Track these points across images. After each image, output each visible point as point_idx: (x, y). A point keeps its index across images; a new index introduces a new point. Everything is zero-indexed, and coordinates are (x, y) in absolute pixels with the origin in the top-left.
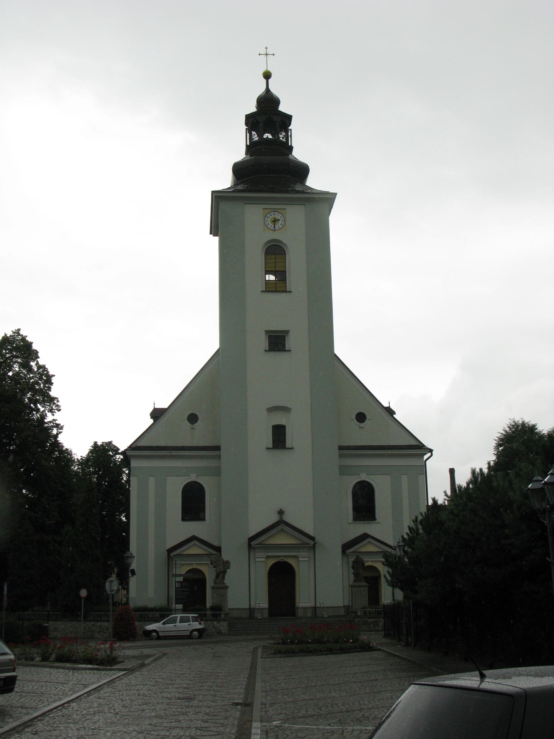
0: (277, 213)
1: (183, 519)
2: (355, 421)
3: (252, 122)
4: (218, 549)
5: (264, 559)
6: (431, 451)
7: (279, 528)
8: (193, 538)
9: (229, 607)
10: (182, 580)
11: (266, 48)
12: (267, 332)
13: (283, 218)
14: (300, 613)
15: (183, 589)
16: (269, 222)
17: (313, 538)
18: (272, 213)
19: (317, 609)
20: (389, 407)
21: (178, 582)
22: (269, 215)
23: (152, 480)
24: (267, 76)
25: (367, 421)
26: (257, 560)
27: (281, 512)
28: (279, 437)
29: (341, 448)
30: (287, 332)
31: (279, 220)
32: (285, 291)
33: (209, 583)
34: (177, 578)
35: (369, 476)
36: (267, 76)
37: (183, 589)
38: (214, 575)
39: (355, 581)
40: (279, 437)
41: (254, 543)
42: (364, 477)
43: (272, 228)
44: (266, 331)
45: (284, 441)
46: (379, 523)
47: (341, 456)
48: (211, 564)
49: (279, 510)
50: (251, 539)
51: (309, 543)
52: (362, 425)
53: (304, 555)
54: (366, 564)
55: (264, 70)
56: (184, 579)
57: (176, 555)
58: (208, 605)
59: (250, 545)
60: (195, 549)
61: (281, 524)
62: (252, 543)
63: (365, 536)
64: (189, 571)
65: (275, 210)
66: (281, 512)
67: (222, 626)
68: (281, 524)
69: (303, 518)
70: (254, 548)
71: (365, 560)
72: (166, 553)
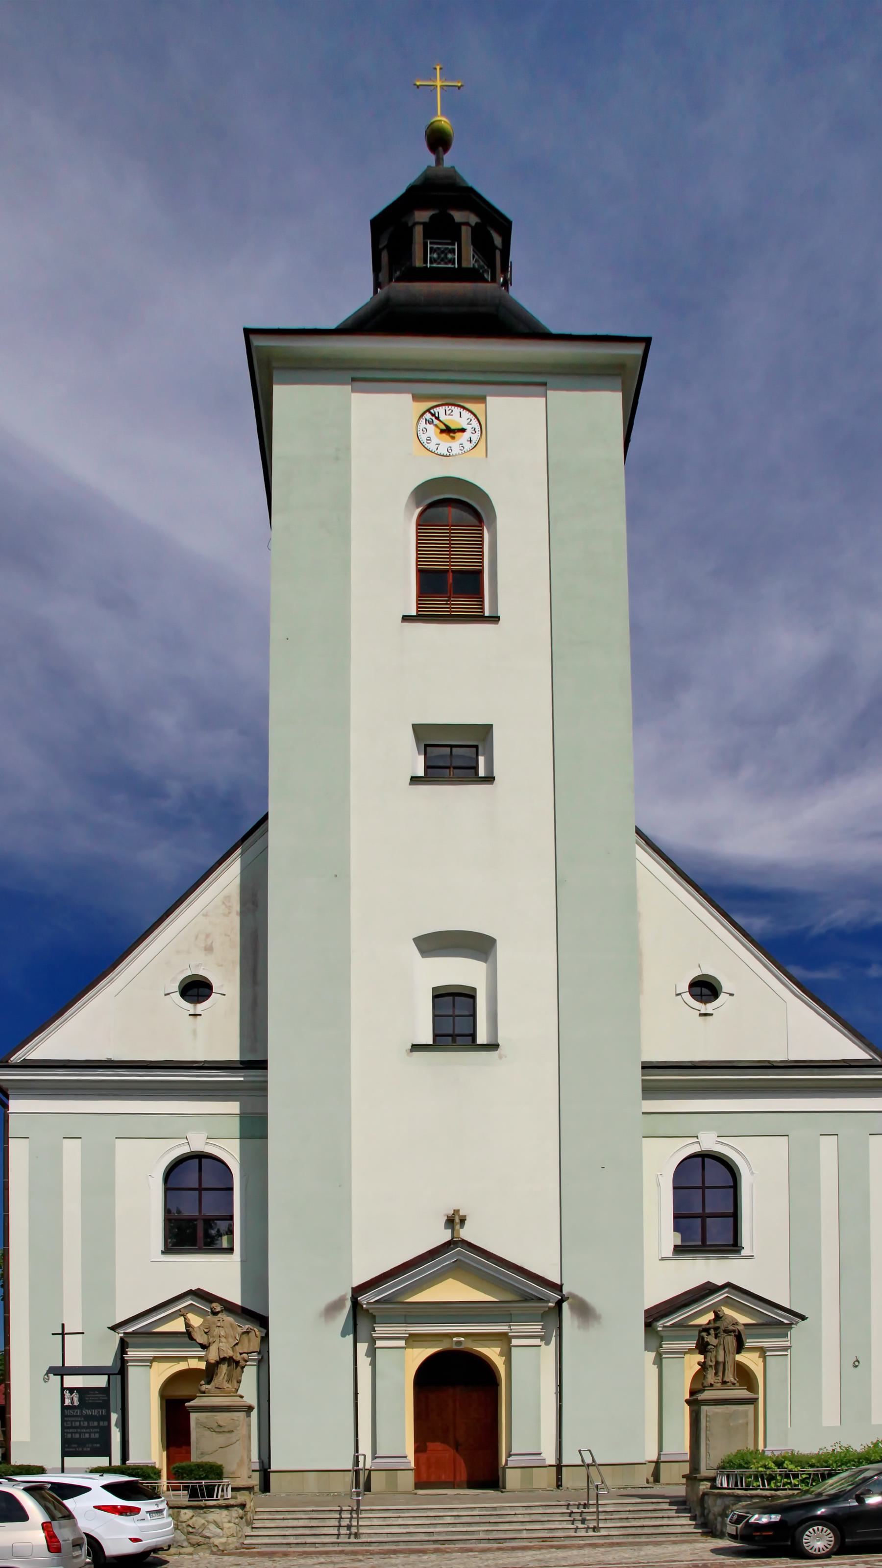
0: (457, 410)
2: (687, 997)
3: (390, 233)
5: (402, 1343)
12: (419, 730)
13: (475, 423)
15: (89, 1412)
17: (558, 1288)
21: (71, 1390)
23: (72, 1150)
24: (438, 141)
25: (723, 997)
26: (379, 1343)
27: (454, 1221)
28: (455, 1022)
29: (647, 1067)
31: (463, 430)
32: (480, 618)
37: (89, 1412)
42: (709, 1142)
47: (650, 1091)
51: (542, 1302)
52: (709, 1008)
57: (134, 1333)
59: (355, 1304)
61: (456, 1252)
62: (363, 1299)
63: (708, 1290)
66: (454, 1221)
67: (216, 1523)
68: (456, 1252)
70: (373, 1319)
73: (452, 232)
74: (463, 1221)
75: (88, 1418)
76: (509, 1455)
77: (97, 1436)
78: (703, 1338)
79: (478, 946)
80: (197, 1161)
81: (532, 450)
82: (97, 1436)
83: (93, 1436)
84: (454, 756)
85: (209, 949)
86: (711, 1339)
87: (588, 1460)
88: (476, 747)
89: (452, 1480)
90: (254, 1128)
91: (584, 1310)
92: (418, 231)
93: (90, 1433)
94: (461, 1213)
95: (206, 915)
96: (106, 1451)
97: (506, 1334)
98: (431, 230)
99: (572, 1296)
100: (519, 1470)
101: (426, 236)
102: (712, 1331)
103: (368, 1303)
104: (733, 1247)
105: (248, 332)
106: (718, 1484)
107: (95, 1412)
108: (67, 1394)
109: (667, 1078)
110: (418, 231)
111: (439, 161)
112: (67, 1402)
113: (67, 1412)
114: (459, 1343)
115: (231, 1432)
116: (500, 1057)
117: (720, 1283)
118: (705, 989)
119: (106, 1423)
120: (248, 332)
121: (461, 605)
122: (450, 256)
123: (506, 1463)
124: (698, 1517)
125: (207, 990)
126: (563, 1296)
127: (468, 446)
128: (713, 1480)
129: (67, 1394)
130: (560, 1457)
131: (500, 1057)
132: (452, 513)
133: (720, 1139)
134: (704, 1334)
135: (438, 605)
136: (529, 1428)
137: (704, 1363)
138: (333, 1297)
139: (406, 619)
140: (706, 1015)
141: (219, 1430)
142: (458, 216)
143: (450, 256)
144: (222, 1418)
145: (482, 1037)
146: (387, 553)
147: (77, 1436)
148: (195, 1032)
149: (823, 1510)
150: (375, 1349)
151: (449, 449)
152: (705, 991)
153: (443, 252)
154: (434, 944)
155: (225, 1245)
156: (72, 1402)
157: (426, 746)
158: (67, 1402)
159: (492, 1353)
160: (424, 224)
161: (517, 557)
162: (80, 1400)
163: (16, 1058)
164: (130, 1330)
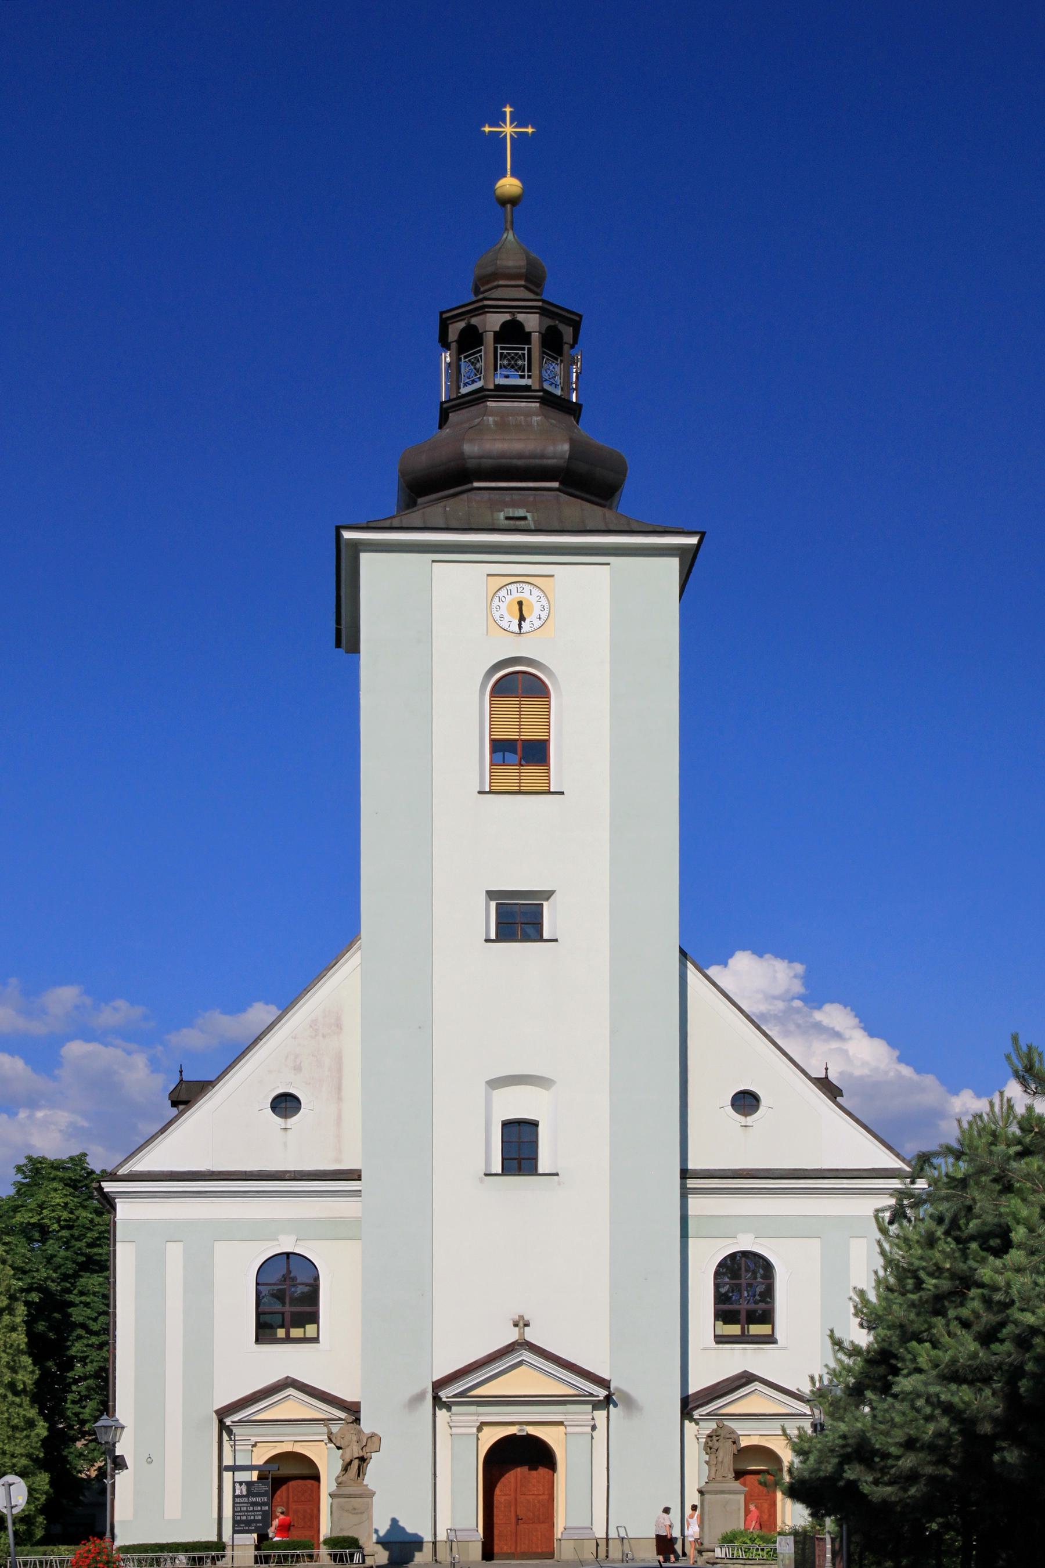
0: (527, 587)
1: (258, 1340)
4: (353, 1410)
8: (290, 1383)
9: (372, 568)
10: (255, 1478)
14: (565, 1551)
15: (254, 1499)
16: (504, 610)
17: (603, 1383)
18: (513, 587)
20: (826, 1078)
21: (241, 1483)
22: (503, 592)
23: (175, 1252)
30: (548, 895)
33: (327, 1485)
34: (739, 1332)
35: (758, 1240)
37: (254, 1499)
38: (339, 1465)
41: (443, 1393)
42: (745, 1243)
43: (517, 630)
44: (488, 892)
45: (535, 1159)
48: (331, 1440)
50: (439, 1385)
54: (744, 1443)
56: (260, 1478)
57: (240, 1421)
58: (325, 1530)
60: (292, 1406)
62: (444, 1394)
63: (746, 1379)
71: (740, 1433)
72: (215, 1416)
75: (253, 1504)
81: (604, 619)
85: (298, 1069)
87: (623, 1534)
89: (513, 1551)
91: (630, 1403)
92: (489, 338)
95: (295, 1038)
99: (617, 1389)
107: (259, 1499)
108: (237, 1485)
112: (238, 1492)
113: (237, 1500)
115: (362, 1513)
116: (559, 1184)
118: (746, 1102)
121: (531, 774)
122: (520, 362)
125: (294, 1104)
126: (610, 1392)
129: (237, 1485)
131: (559, 1184)
132: (518, 684)
135: (510, 775)
138: (416, 1390)
143: (520, 362)
146: (462, 724)
148: (285, 1144)
152: (750, 1100)
153: (513, 358)
158: (238, 1492)
160: (495, 332)
161: (578, 725)
163: (123, 1171)
164: (236, 1419)
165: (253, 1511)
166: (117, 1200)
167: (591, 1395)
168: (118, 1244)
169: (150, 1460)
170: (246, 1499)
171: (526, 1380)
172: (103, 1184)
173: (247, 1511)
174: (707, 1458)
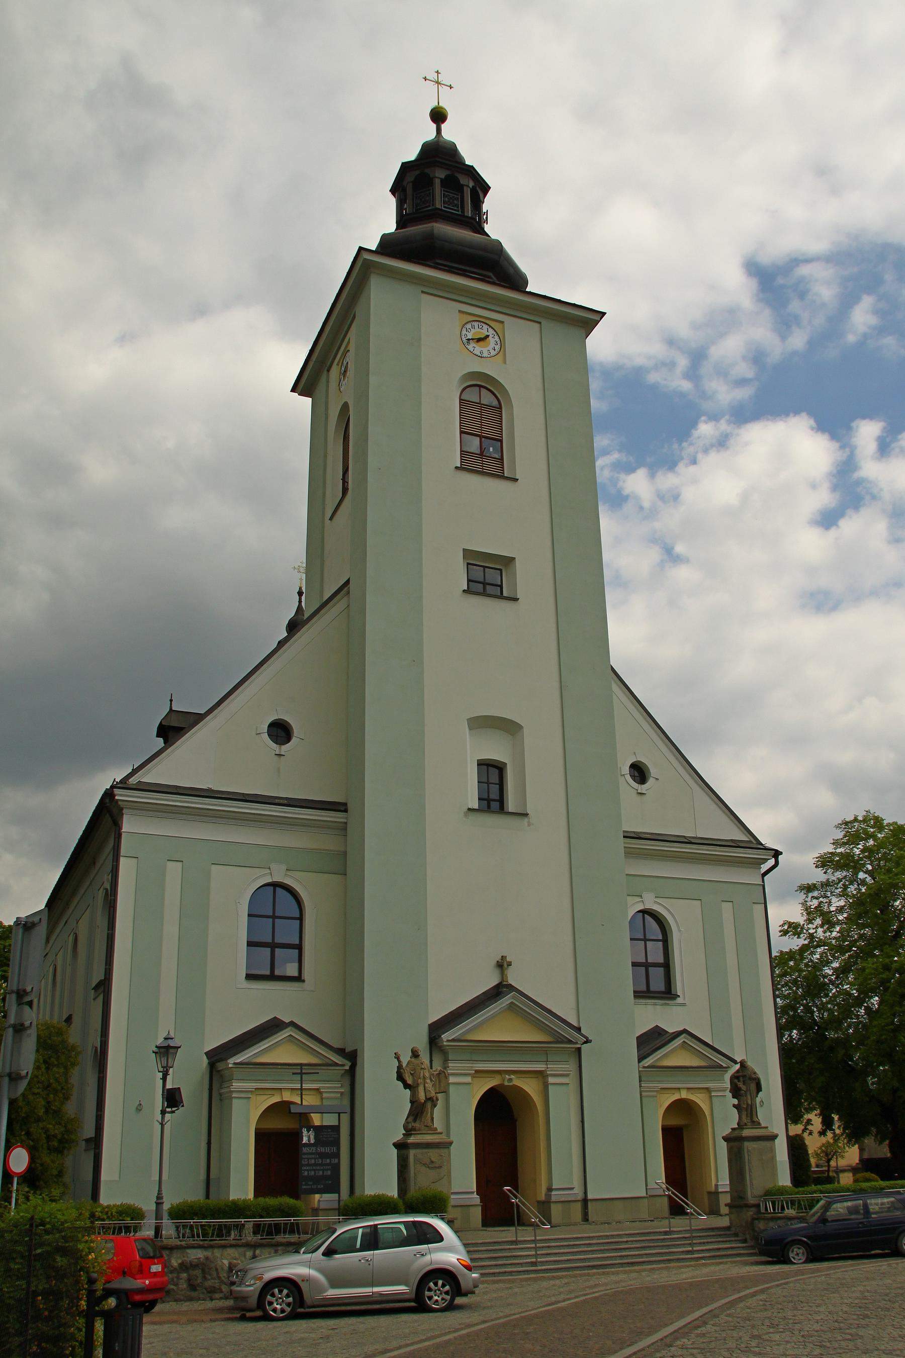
5: (468, 1079)
6: (777, 854)
7: (505, 1001)
8: (273, 1026)
11: (437, 72)
12: (467, 553)
15: (323, 1150)
18: (476, 324)
19: (590, 1206)
22: (469, 326)
23: (174, 870)
24: (438, 116)
25: (651, 782)
27: (502, 965)
28: (494, 790)
29: (627, 836)
36: (438, 116)
37: (323, 1150)
39: (741, 1126)
40: (494, 790)
46: (684, 1005)
47: (629, 853)
49: (498, 958)
50: (436, 1029)
51: (565, 1041)
53: (560, 1070)
55: (434, 104)
60: (279, 1051)
64: (271, 1110)
65: (483, 321)
66: (502, 965)
69: (547, 983)
72: (205, 1061)
73: (460, 188)
74: (509, 964)
75: (322, 1155)
76: (550, 1189)
77: (329, 1173)
78: (736, 1085)
79: (509, 728)
80: (272, 888)
82: (329, 1173)
83: (325, 1173)
84: (488, 577)
86: (740, 1085)
88: (501, 570)
90: (343, 864)
92: (437, 183)
93: (323, 1170)
94: (508, 959)
96: (334, 1188)
97: (541, 1072)
98: (445, 183)
100: (459, 1209)
101: (442, 186)
102: (741, 1079)
103: (448, 1041)
104: (668, 993)
105: (361, 249)
106: (763, 1210)
107: (328, 1150)
109: (642, 844)
110: (437, 183)
111: (439, 131)
114: (510, 1080)
115: (440, 1167)
117: (287, 1020)
119: (336, 1161)
120: (361, 249)
123: (548, 1195)
124: (749, 1240)
127: (493, 353)
128: (758, 1206)
130: (586, 1193)
133: (658, 900)
134: (736, 1081)
136: (559, 1162)
137: (739, 1104)
139: (456, 468)
140: (641, 794)
141: (431, 1165)
142: (463, 180)
144: (433, 1154)
145: (511, 806)
147: (313, 1173)
149: (473, 1275)
150: (449, 1084)
151: (481, 352)
154: (484, 724)
155: (291, 970)
156: (309, 1140)
157: (468, 564)
159: (530, 1087)
162: (315, 1138)
165: (322, 1165)
166: (125, 811)
167: (570, 1042)
168: (122, 860)
169: (139, 1108)
170: (313, 1149)
171: (495, 1027)
172: (116, 791)
173: (315, 1165)
174: (736, 1101)
